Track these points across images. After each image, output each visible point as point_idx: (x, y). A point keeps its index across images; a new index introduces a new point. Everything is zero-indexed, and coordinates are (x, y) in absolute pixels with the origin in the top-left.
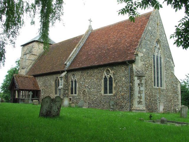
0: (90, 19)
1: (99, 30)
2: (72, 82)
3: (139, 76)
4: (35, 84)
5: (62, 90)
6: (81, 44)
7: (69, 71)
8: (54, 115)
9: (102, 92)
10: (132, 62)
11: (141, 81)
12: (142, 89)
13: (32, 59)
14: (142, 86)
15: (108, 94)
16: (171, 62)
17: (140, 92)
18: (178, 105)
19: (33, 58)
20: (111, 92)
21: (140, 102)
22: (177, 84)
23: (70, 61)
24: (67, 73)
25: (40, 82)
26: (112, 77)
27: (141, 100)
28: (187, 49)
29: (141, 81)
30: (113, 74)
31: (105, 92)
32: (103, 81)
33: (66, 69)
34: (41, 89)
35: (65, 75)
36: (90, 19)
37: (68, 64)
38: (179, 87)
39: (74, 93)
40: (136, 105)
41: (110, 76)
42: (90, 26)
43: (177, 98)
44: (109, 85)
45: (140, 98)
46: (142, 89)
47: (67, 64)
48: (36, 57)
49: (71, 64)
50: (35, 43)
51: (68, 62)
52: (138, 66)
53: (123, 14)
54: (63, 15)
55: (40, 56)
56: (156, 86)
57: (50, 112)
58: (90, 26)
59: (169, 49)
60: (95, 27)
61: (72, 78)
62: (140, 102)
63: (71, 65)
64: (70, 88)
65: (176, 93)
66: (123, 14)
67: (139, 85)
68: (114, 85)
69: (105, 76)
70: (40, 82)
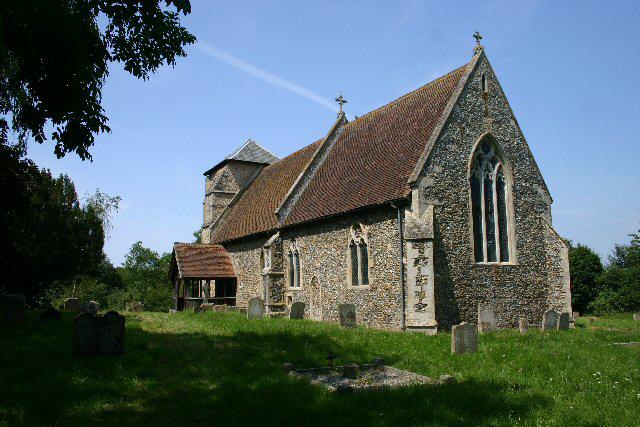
1: (379, 117)
4: (223, 262)
8: (616, 288)
10: (406, 203)
15: (361, 287)
16: (540, 191)
20: (365, 281)
21: (420, 307)
25: (237, 263)
26: (366, 241)
27: (424, 302)
28: (90, 150)
30: (369, 234)
31: (355, 282)
32: (349, 252)
39: (295, 282)
41: (362, 240)
44: (361, 258)
45: (420, 295)
53: (186, 48)
56: (485, 259)
61: (290, 247)
62: (420, 307)
66: (186, 48)
68: (371, 263)
69: (353, 241)
70: (237, 263)
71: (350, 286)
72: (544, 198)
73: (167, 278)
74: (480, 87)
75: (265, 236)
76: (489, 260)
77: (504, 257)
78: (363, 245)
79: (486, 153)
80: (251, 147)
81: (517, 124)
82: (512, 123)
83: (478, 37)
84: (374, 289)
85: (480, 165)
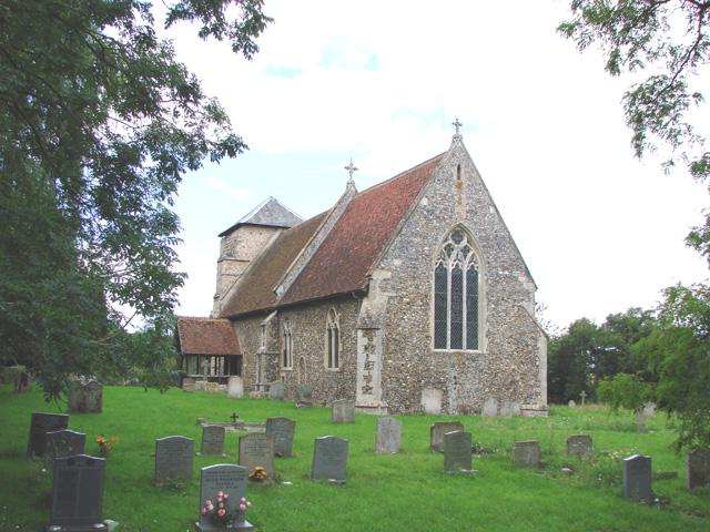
0: (351, 164)
2: (330, 331)
3: (367, 329)
5: (263, 356)
6: (320, 236)
7: (282, 310)
9: (326, 364)
10: (363, 294)
11: (370, 339)
12: (372, 358)
13: (236, 272)
14: (373, 352)
15: (334, 369)
16: (522, 279)
17: (368, 366)
18: (537, 394)
19: (238, 269)
21: (367, 390)
22: (535, 340)
23: (288, 284)
24: (277, 315)
27: (371, 385)
29: (370, 339)
32: (327, 332)
33: (275, 305)
34: (242, 351)
35: (272, 321)
36: (351, 164)
37: (281, 291)
38: (542, 345)
40: (361, 399)
42: (351, 184)
43: (536, 375)
45: (368, 379)
46: (372, 358)
47: (278, 292)
48: (247, 267)
49: (290, 289)
50: (242, 230)
51: (281, 287)
52: (374, 304)
54: (560, 38)
55: (256, 264)
56: (449, 347)
57: (84, 404)
58: (351, 184)
59: (514, 243)
60: (362, 186)
61: (288, 327)
63: (288, 294)
64: (282, 352)
65: (533, 361)
67: (366, 348)
71: (327, 369)
72: (527, 286)
73: (171, 356)
74: (455, 177)
75: (263, 313)
76: (468, 348)
77: (473, 344)
78: (336, 330)
79: (458, 242)
80: (273, 206)
81: (497, 210)
82: (492, 210)
83: (457, 125)
84: (341, 372)
85: (449, 256)
